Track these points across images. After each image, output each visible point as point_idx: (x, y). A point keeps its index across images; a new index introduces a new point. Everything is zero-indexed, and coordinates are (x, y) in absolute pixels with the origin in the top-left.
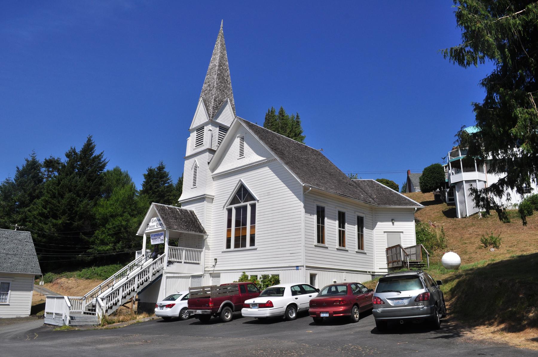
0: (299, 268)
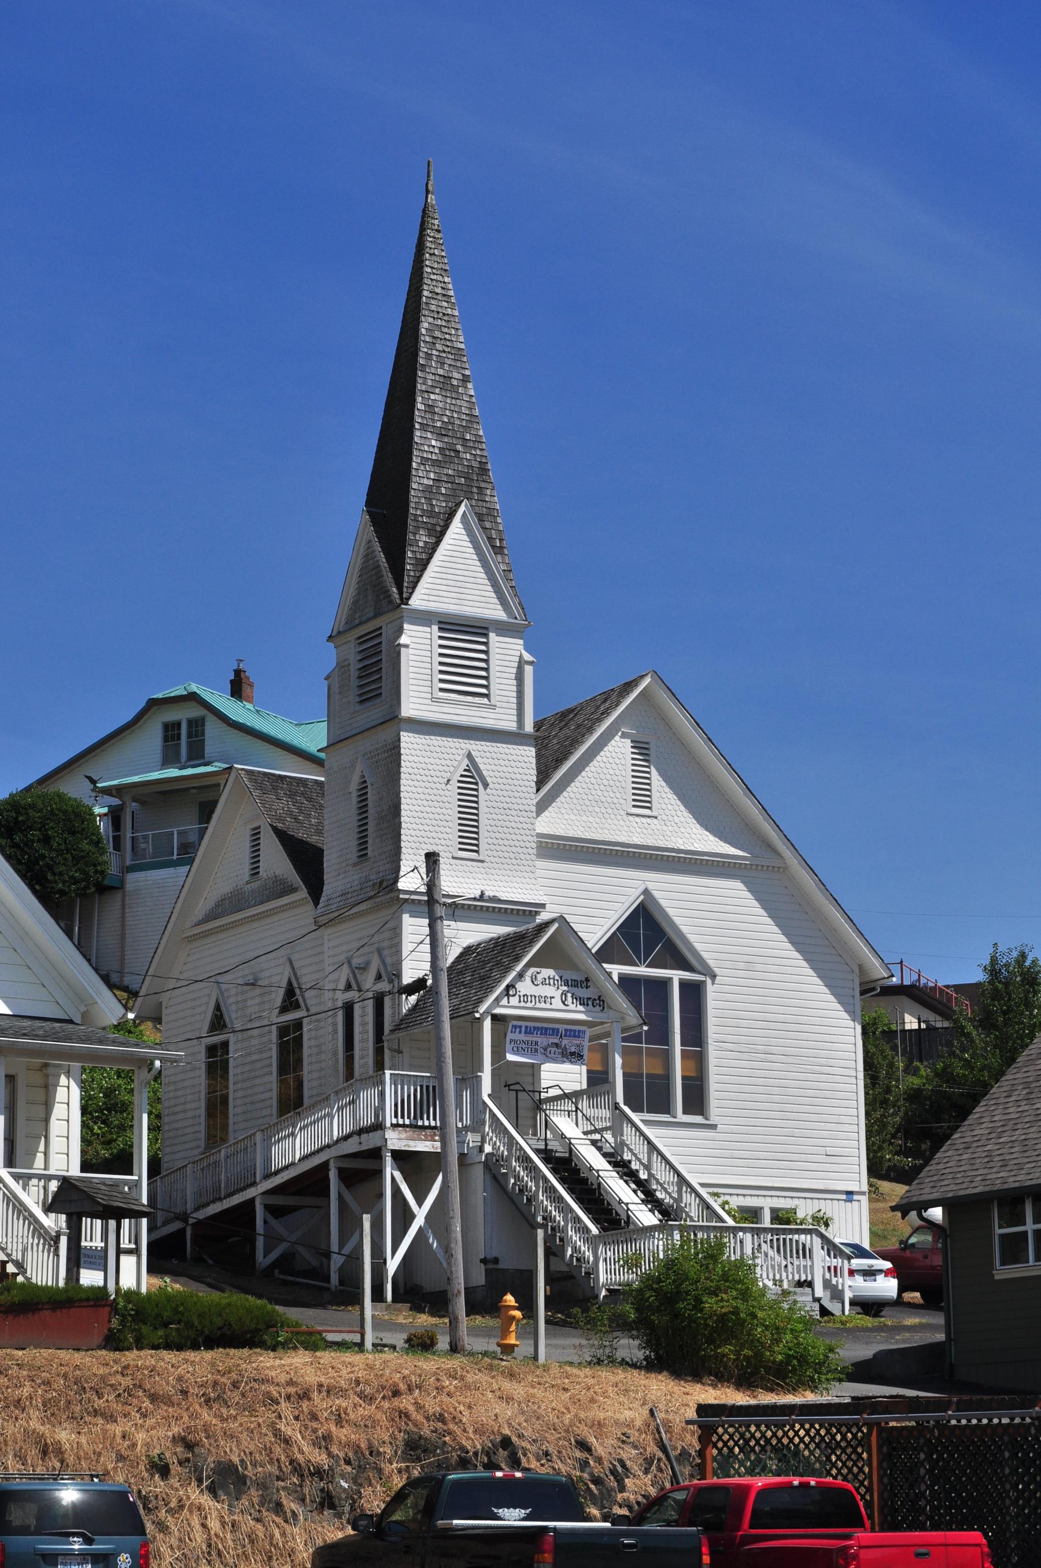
0: (855, 1197)
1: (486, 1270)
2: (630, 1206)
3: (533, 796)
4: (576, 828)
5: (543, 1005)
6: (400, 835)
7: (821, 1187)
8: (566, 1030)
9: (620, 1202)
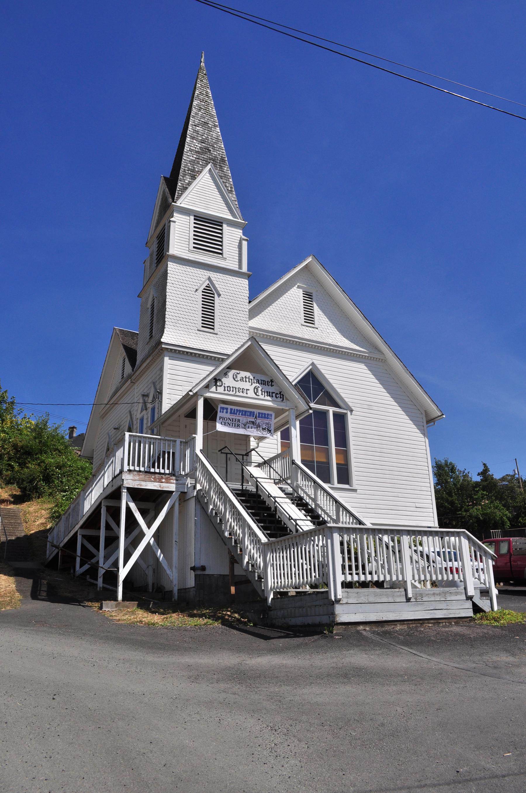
1: (195, 575)
2: (298, 522)
3: (247, 307)
4: (273, 328)
5: (241, 394)
6: (165, 314)
7: (414, 525)
8: (259, 413)
9: (290, 518)
